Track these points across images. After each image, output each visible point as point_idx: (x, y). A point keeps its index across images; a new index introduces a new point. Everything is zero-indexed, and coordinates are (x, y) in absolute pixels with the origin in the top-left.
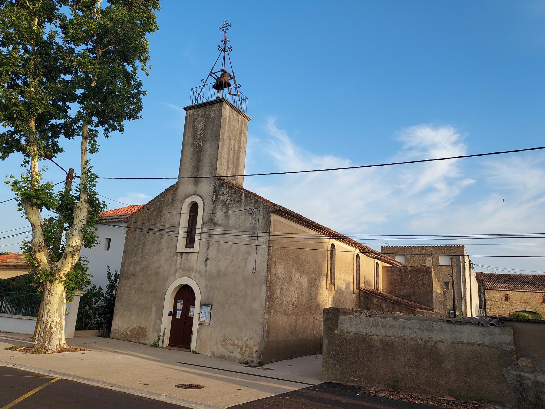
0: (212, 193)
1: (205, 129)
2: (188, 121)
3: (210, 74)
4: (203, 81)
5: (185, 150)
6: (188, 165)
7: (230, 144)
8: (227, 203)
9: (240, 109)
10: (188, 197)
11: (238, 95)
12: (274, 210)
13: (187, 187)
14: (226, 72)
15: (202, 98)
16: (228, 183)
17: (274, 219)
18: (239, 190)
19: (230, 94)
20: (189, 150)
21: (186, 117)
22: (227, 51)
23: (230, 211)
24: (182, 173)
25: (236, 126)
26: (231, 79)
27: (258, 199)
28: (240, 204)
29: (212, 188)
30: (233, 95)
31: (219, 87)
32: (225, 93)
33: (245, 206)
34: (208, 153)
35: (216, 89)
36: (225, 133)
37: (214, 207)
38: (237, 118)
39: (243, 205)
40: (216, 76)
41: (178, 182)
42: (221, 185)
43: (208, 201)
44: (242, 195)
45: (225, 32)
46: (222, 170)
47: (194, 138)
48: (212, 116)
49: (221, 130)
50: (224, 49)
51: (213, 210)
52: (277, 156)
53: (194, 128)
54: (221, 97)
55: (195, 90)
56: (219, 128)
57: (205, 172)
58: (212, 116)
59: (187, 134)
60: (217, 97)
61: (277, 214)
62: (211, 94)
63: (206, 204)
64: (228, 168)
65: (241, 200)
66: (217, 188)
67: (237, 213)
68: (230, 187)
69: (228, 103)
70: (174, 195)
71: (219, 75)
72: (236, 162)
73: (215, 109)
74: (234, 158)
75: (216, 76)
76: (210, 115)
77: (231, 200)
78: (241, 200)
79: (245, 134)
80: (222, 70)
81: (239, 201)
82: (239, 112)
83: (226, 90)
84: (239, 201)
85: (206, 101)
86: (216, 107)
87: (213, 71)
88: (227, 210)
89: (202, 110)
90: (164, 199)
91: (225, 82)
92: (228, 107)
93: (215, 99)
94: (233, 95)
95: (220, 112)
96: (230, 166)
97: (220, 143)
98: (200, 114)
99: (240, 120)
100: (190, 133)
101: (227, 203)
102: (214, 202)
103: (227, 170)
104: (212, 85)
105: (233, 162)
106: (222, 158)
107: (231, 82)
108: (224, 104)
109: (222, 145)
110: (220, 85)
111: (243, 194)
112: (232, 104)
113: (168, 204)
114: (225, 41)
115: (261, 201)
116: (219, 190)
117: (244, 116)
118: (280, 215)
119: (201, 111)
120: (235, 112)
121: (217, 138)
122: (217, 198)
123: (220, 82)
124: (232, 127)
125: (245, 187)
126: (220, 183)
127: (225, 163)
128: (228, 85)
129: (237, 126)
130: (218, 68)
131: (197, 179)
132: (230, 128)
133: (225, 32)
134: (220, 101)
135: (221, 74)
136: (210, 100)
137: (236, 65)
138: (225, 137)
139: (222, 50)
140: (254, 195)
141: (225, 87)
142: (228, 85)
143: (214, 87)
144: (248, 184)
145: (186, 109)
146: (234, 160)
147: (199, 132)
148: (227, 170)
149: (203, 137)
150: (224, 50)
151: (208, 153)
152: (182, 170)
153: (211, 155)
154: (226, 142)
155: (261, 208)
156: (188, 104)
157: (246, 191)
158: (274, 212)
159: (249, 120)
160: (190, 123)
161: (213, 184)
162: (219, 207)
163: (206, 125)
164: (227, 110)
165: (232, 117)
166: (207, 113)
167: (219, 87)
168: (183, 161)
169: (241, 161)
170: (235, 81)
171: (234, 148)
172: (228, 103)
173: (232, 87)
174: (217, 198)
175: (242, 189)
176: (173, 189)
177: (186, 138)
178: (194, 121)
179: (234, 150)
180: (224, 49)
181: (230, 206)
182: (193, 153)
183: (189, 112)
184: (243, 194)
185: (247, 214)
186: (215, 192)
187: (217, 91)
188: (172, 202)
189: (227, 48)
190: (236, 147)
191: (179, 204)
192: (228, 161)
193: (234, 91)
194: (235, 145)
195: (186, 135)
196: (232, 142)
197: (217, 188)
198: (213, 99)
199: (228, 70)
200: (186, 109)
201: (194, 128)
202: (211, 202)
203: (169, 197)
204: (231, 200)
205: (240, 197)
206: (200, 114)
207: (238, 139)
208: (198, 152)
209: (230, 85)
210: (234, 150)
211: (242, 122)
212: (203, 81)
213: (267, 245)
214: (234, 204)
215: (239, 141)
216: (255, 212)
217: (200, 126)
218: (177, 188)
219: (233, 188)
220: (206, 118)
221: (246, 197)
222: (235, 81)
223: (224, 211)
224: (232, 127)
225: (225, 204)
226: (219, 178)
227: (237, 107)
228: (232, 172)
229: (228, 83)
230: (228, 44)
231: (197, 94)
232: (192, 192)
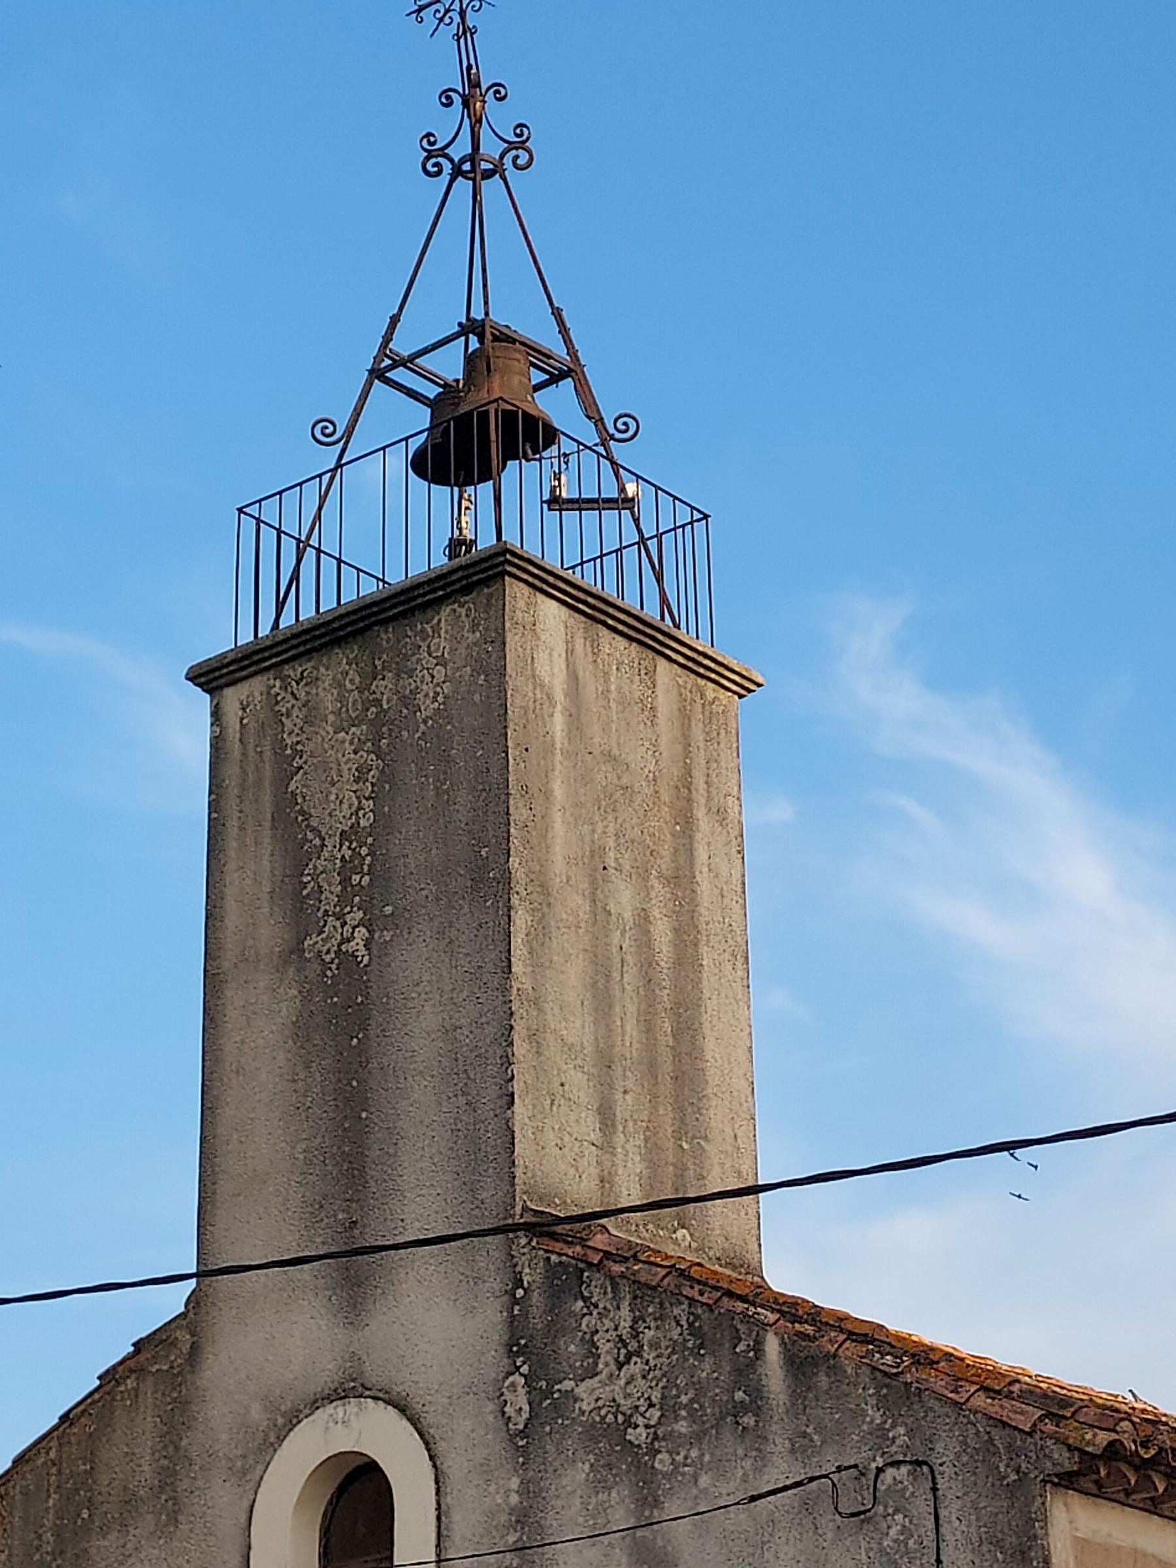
0: (494, 1360)
1: (383, 825)
2: (231, 772)
3: (377, 374)
4: (323, 432)
5: (232, 1015)
6: (269, 1140)
7: (600, 914)
8: (639, 1435)
9: (652, 611)
10: (293, 1420)
11: (625, 503)
12: (1066, 1461)
13: (280, 1336)
14: (504, 337)
15: (328, 565)
16: (630, 1254)
17: (1082, 1545)
18: (727, 1308)
19: (555, 502)
20: (268, 1014)
21: (217, 745)
22: (497, 170)
23: (672, 1507)
24: (222, 1217)
25: (638, 757)
26: (554, 379)
27: (906, 1372)
28: (757, 1437)
29: (491, 1317)
30: (580, 504)
31: (464, 464)
32: (514, 508)
33: (800, 1446)
34: (429, 1019)
35: (439, 478)
36: (555, 833)
37: (525, 1490)
38: (637, 689)
39: (779, 1443)
40: (429, 377)
41: (194, 1301)
42: (566, 1282)
43: (471, 1435)
44: (758, 1347)
45: (465, 32)
46: (568, 1154)
47: (300, 907)
48: (428, 707)
49: (518, 811)
50: (474, 157)
51: (522, 1518)
52: (971, 920)
53: (290, 818)
54: (486, 541)
55: (269, 512)
56: (495, 795)
57: (420, 1197)
58: (428, 707)
59: (234, 883)
60: (456, 545)
61: (1099, 1492)
62: (393, 528)
63: (454, 1465)
64: (606, 1118)
65: (757, 1394)
66: (537, 1320)
67: (740, 1517)
68: (643, 1291)
69: (546, 582)
70: (178, 1415)
71: (450, 364)
72: (677, 1069)
73: (442, 644)
74: (648, 1026)
75: (429, 377)
76: (408, 701)
77: (669, 1410)
78: (757, 1402)
79: (721, 814)
80: (471, 327)
81: (743, 1410)
82: (650, 638)
83: (522, 479)
84: (743, 1410)
85: (369, 588)
86: (448, 631)
87: (402, 345)
88: (648, 1498)
89: (334, 674)
90: (91, 1457)
91: (509, 417)
92: (551, 612)
93: (440, 560)
94: (580, 504)
95: (491, 667)
96: (624, 1105)
97: (521, 919)
98: (328, 700)
99: (665, 703)
100: (257, 866)
101: (639, 1435)
102: (525, 1442)
103: (606, 1146)
104: (398, 461)
105: (652, 1068)
106: (552, 1049)
107: (556, 404)
108: (516, 592)
109: (540, 933)
110: (467, 442)
111: (772, 1346)
112: (587, 578)
113: (130, 1503)
114: (471, 95)
115: (939, 1384)
116: (554, 1329)
117: (699, 665)
118: (1125, 1498)
119: (332, 678)
120: (614, 647)
121: (486, 877)
122: (547, 1404)
123: (464, 421)
124: (604, 776)
125: (784, 1275)
126: (559, 1261)
127: (580, 1085)
128: (530, 435)
129: (647, 753)
130: (435, 314)
131: (353, 1260)
132: (586, 779)
133: (471, 95)
134: (476, 576)
135: (470, 360)
136: (396, 577)
137: (583, 268)
138: (558, 864)
139: (457, 172)
140: (869, 1336)
141: (510, 453)
142: (530, 435)
143: (419, 464)
144: (809, 1255)
145: (211, 677)
146: (650, 1045)
147: (335, 852)
148: (606, 1146)
149: (370, 885)
150: (472, 169)
151: (429, 1019)
152: (225, 1187)
153: (449, 1031)
154: (572, 904)
155: (945, 1451)
156: (221, 638)
157: (793, 1310)
158: (1067, 1481)
159: (746, 686)
160: (252, 792)
161: (495, 1283)
162: (572, 1481)
163: (383, 788)
164: (544, 633)
165: (591, 687)
166: (384, 686)
167: (464, 464)
168: (228, 1114)
169: (712, 1049)
170: (583, 391)
171: (645, 940)
172: (546, 582)
173: (567, 446)
174: (547, 1404)
175: (760, 1295)
176: (159, 1368)
177: (233, 918)
178: (287, 764)
179: (648, 965)
180: (474, 157)
181: (662, 1462)
182: (300, 1032)
183: (232, 697)
184: (772, 1346)
185: (828, 1522)
186: (524, 1347)
187: (441, 493)
188: (167, 1479)
189: (491, 148)
190: (662, 931)
191: (219, 1498)
192: (606, 1061)
193: (586, 477)
194: (644, 919)
195: (231, 893)
196: (623, 898)
197: (537, 1320)
198: (419, 568)
199: (519, 312)
200: (211, 677)
201: (290, 818)
202: (494, 1443)
203: (132, 1452)
204: (669, 1410)
205: (746, 1370)
206: (328, 700)
207: (665, 863)
208: (342, 1020)
209: (551, 435)
210: (648, 965)
211: (684, 716)
212: (323, 432)
213: (940, 1493)
214: (697, 1438)
215: (682, 880)
216: (896, 1489)
217: (337, 803)
218: (195, 1348)
219: (677, 1296)
220: (381, 729)
221: (800, 1365)
222: (583, 391)
223: (621, 1518)
224: (604, 776)
225: (619, 1448)
226: (542, 1228)
227: (631, 601)
228: (653, 1161)
229: (531, 421)
230: (500, 119)
231: (289, 546)
232: (327, 1374)
